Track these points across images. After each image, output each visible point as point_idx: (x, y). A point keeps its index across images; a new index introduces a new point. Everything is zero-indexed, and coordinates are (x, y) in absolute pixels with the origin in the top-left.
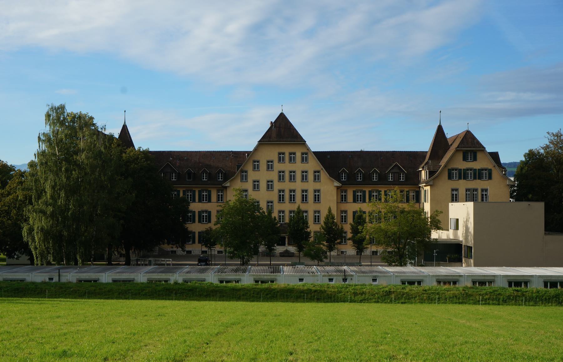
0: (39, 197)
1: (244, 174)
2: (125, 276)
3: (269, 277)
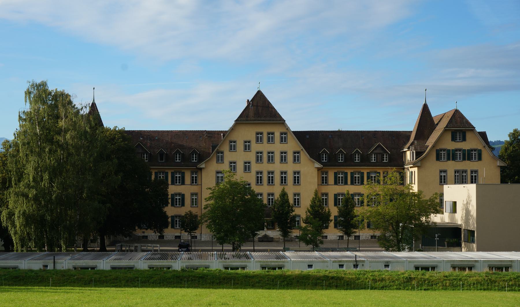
0: (20, 179)
1: (220, 155)
3: (277, 264)
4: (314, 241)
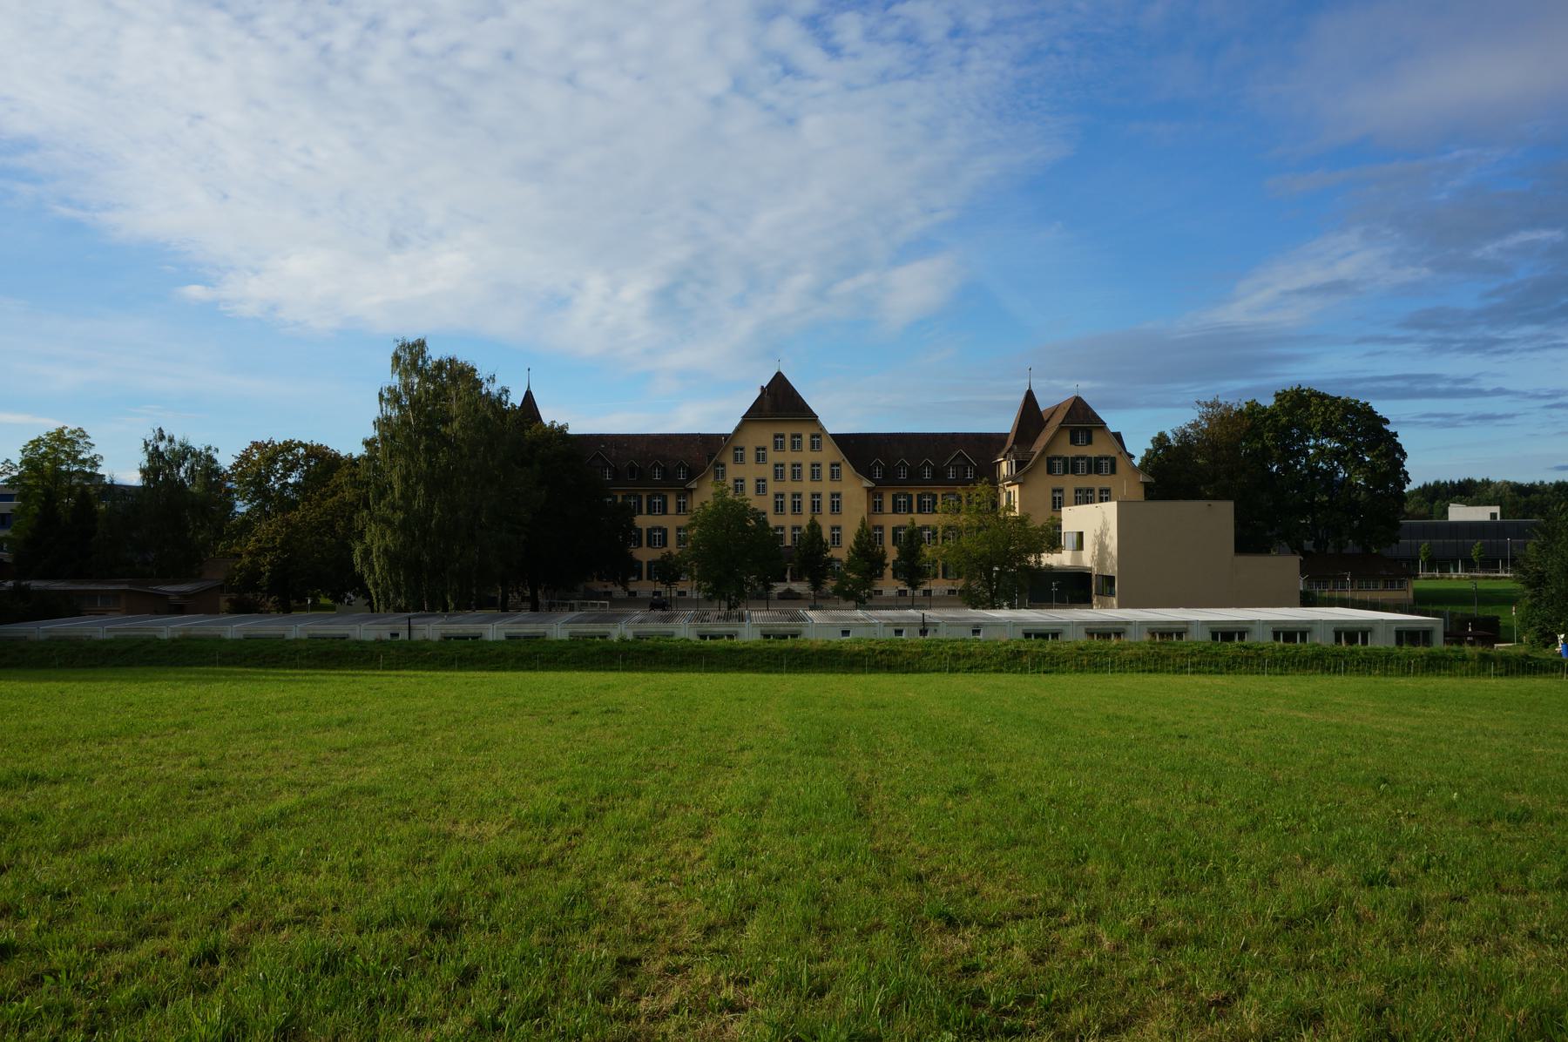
0: (381, 495)
2: (528, 629)
4: (859, 595)
